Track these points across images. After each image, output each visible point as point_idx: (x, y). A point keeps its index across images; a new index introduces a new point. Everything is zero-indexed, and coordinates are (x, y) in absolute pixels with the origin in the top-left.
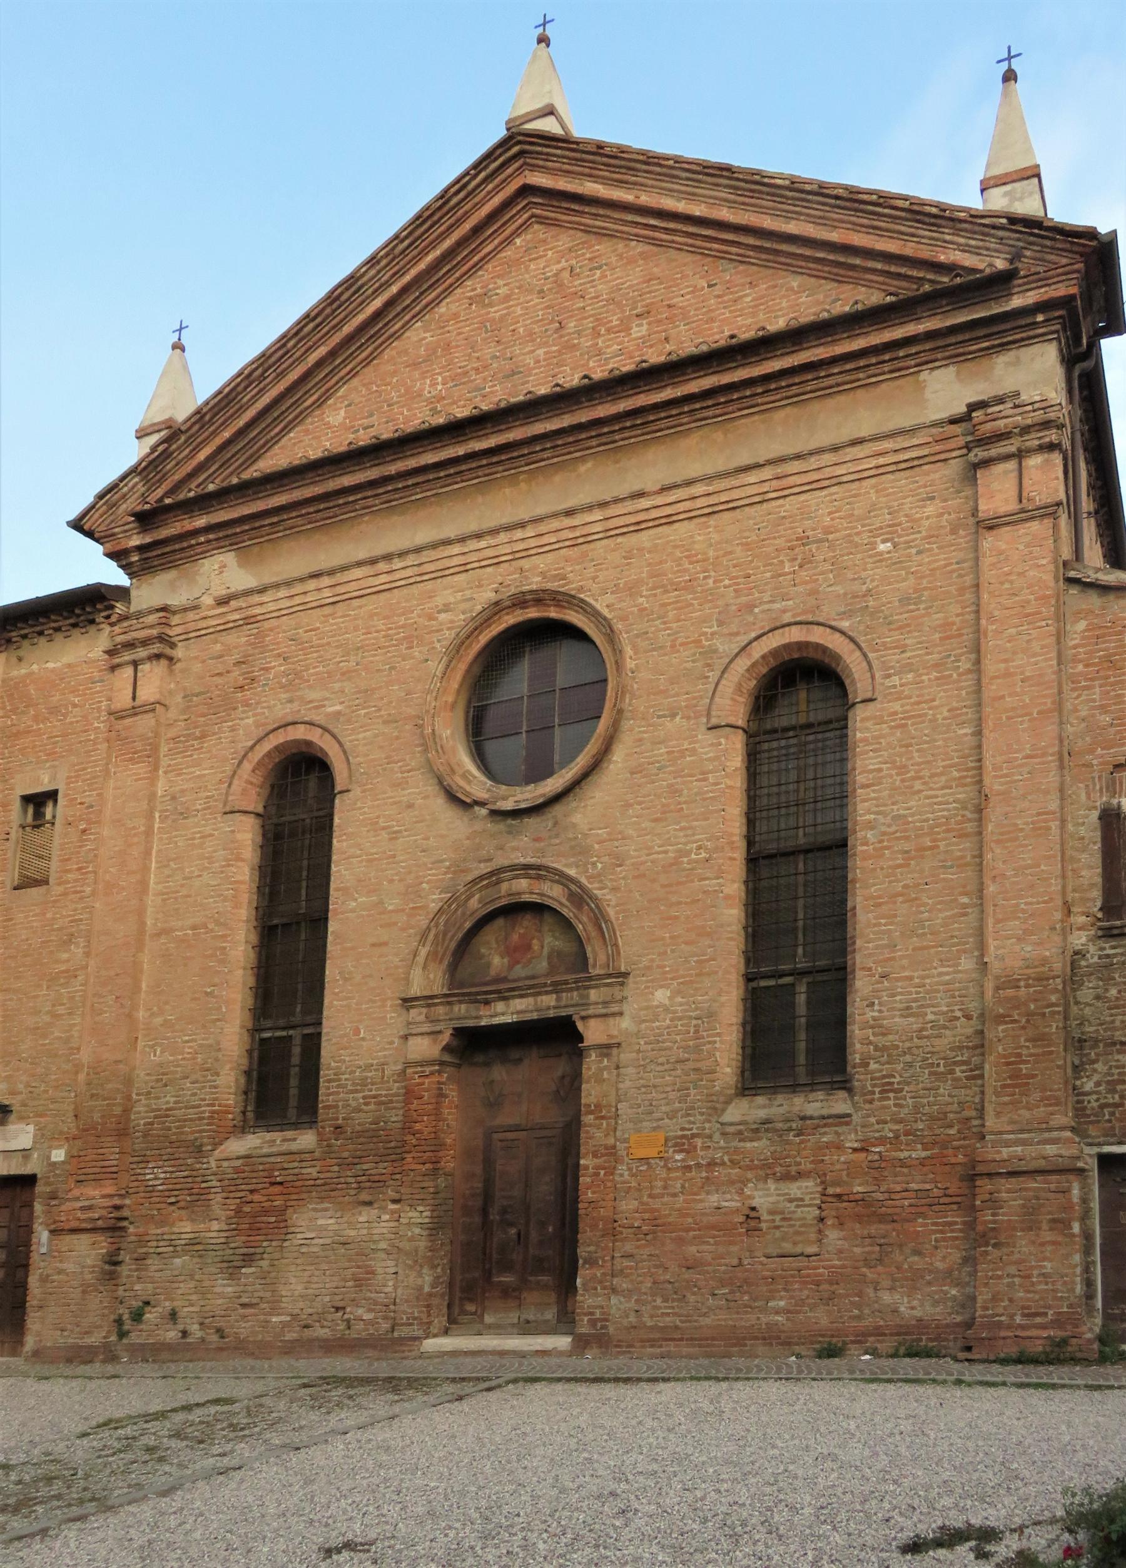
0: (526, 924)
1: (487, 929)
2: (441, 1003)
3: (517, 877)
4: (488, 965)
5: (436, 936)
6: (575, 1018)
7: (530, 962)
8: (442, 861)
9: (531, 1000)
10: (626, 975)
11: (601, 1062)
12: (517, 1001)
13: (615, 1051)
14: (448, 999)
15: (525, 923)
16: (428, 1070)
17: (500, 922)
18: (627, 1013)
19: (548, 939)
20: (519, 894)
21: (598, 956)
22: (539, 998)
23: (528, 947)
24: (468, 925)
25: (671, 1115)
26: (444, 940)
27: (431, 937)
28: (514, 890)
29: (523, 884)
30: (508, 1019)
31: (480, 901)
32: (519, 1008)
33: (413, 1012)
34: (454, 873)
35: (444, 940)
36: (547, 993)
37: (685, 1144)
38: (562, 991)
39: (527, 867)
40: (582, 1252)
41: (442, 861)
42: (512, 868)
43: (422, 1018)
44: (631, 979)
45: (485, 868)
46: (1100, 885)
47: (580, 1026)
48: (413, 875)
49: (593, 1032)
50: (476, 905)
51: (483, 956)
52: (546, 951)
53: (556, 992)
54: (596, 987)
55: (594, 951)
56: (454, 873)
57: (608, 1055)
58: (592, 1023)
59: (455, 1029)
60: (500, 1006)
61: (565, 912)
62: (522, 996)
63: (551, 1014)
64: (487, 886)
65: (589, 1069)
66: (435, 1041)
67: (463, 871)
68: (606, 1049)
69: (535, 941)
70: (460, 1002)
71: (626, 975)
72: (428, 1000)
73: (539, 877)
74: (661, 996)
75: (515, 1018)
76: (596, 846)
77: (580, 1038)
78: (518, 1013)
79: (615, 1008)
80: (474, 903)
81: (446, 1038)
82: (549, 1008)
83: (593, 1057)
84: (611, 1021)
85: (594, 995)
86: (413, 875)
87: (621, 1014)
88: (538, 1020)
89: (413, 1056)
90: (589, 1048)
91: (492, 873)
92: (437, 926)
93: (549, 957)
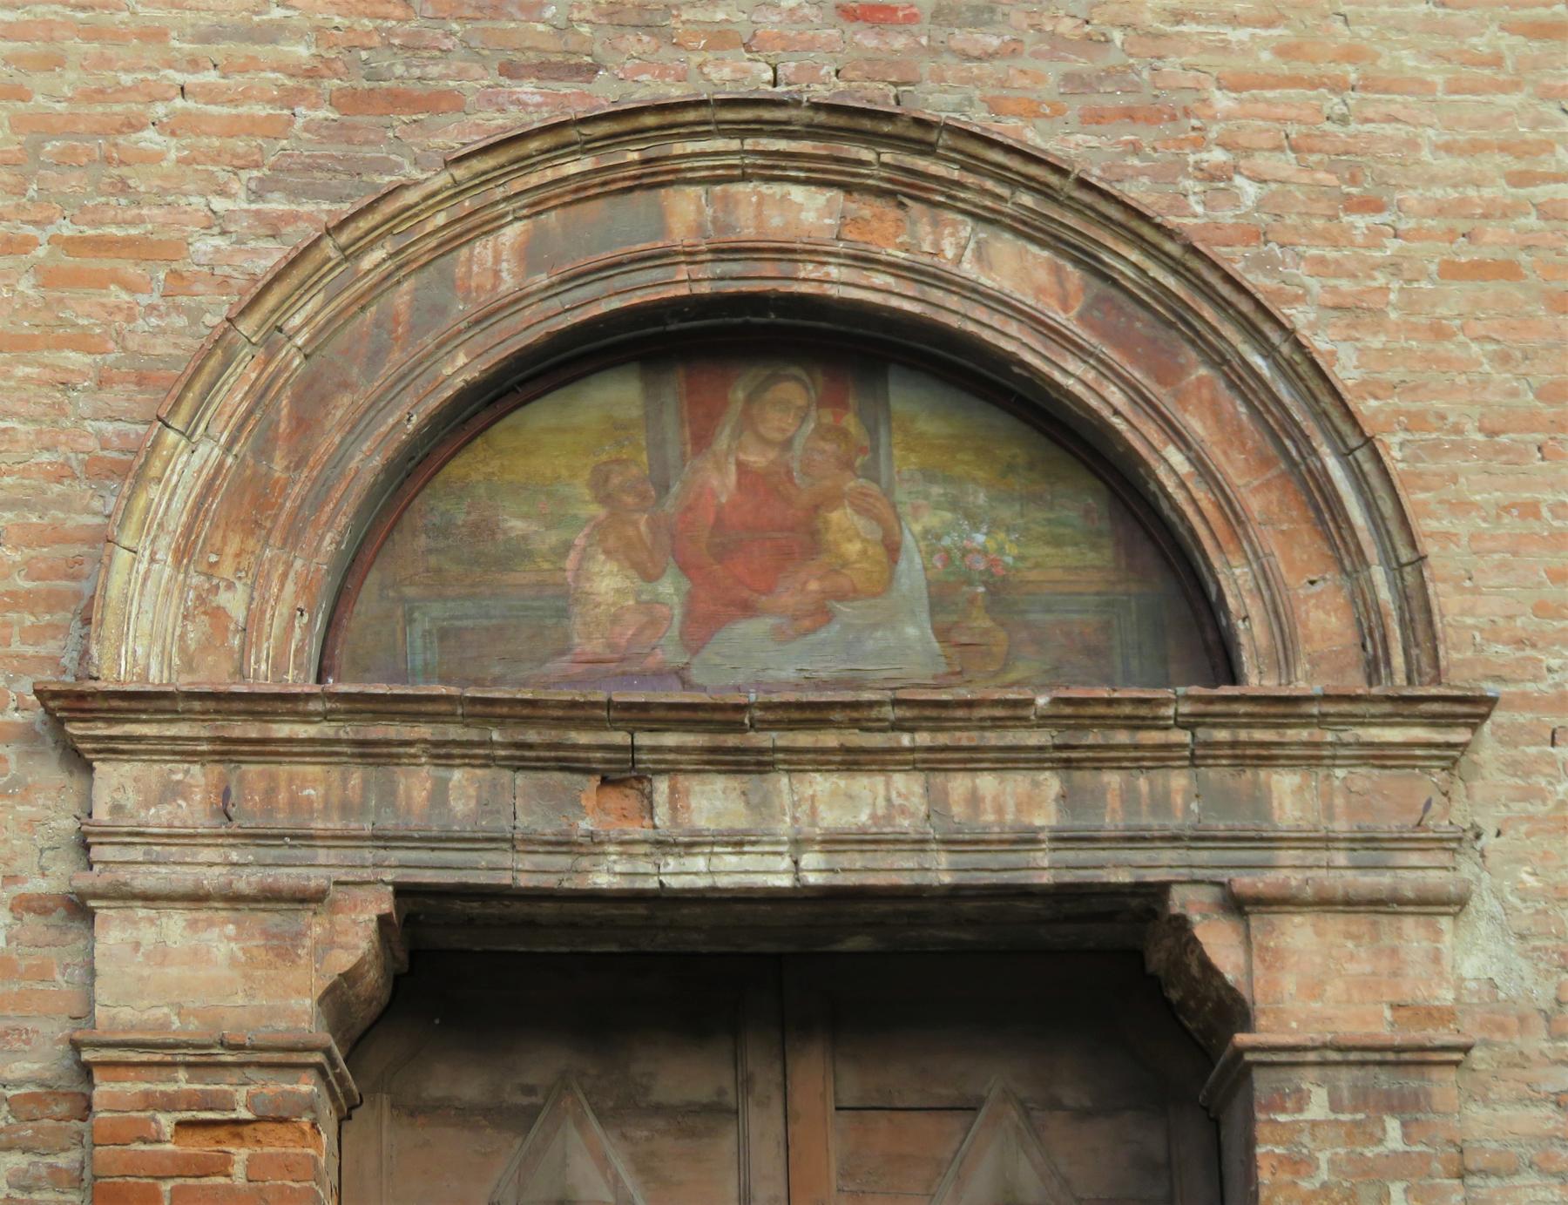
0: (779, 424)
1: (540, 416)
2: (321, 750)
3: (772, 170)
4: (563, 601)
5: (260, 396)
6: (1182, 900)
7: (822, 614)
8: (270, 34)
9: (906, 787)
10: (1473, 709)
11: (1367, 1133)
12: (821, 784)
13: (1443, 1084)
14: (374, 721)
15: (775, 422)
16: (242, 1095)
17: (616, 396)
18: (1484, 903)
19: (925, 519)
20: (784, 252)
21: (1289, 607)
22: (958, 785)
23: (803, 541)
24: (460, 368)
26: (304, 425)
27: (234, 394)
28: (746, 230)
29: (808, 210)
30: (772, 872)
31: (530, 256)
32: (831, 818)
33: (115, 782)
34: (349, 101)
35: (304, 425)
36: (1009, 760)
38: (1102, 759)
39: (847, 121)
41: (270, 34)
42: (746, 114)
43: (192, 811)
44: (1488, 746)
45: (533, 101)
46: (1256, 1109)
47: (1220, 945)
48: (70, 80)
49: (1300, 983)
50: (514, 276)
51: (519, 552)
52: (913, 570)
53: (1065, 761)
54: (1311, 759)
55: (1265, 577)
56: (349, 101)
57: (1407, 1107)
58: (1298, 935)
59: (402, 891)
60: (712, 801)
61: (1073, 376)
62: (852, 761)
63: (1043, 868)
64: (580, 192)
65: (1299, 1164)
66: (284, 949)
67: (398, 100)
68: (1400, 1065)
69: (842, 517)
70: (443, 754)
71: (1473, 709)
72: (228, 720)
73: (904, 191)
75: (815, 870)
76: (1223, 101)
77: (1233, 1010)
78: (834, 842)
79: (1418, 872)
80: (497, 258)
81: (351, 937)
82: (1027, 839)
83: (1318, 1107)
84: (1411, 933)
85: (1288, 796)
86: (70, 80)
87: (1453, 904)
88: (954, 893)
89: (124, 1008)
90: (1291, 1057)
91: (626, 122)
92: (273, 336)
93: (940, 599)
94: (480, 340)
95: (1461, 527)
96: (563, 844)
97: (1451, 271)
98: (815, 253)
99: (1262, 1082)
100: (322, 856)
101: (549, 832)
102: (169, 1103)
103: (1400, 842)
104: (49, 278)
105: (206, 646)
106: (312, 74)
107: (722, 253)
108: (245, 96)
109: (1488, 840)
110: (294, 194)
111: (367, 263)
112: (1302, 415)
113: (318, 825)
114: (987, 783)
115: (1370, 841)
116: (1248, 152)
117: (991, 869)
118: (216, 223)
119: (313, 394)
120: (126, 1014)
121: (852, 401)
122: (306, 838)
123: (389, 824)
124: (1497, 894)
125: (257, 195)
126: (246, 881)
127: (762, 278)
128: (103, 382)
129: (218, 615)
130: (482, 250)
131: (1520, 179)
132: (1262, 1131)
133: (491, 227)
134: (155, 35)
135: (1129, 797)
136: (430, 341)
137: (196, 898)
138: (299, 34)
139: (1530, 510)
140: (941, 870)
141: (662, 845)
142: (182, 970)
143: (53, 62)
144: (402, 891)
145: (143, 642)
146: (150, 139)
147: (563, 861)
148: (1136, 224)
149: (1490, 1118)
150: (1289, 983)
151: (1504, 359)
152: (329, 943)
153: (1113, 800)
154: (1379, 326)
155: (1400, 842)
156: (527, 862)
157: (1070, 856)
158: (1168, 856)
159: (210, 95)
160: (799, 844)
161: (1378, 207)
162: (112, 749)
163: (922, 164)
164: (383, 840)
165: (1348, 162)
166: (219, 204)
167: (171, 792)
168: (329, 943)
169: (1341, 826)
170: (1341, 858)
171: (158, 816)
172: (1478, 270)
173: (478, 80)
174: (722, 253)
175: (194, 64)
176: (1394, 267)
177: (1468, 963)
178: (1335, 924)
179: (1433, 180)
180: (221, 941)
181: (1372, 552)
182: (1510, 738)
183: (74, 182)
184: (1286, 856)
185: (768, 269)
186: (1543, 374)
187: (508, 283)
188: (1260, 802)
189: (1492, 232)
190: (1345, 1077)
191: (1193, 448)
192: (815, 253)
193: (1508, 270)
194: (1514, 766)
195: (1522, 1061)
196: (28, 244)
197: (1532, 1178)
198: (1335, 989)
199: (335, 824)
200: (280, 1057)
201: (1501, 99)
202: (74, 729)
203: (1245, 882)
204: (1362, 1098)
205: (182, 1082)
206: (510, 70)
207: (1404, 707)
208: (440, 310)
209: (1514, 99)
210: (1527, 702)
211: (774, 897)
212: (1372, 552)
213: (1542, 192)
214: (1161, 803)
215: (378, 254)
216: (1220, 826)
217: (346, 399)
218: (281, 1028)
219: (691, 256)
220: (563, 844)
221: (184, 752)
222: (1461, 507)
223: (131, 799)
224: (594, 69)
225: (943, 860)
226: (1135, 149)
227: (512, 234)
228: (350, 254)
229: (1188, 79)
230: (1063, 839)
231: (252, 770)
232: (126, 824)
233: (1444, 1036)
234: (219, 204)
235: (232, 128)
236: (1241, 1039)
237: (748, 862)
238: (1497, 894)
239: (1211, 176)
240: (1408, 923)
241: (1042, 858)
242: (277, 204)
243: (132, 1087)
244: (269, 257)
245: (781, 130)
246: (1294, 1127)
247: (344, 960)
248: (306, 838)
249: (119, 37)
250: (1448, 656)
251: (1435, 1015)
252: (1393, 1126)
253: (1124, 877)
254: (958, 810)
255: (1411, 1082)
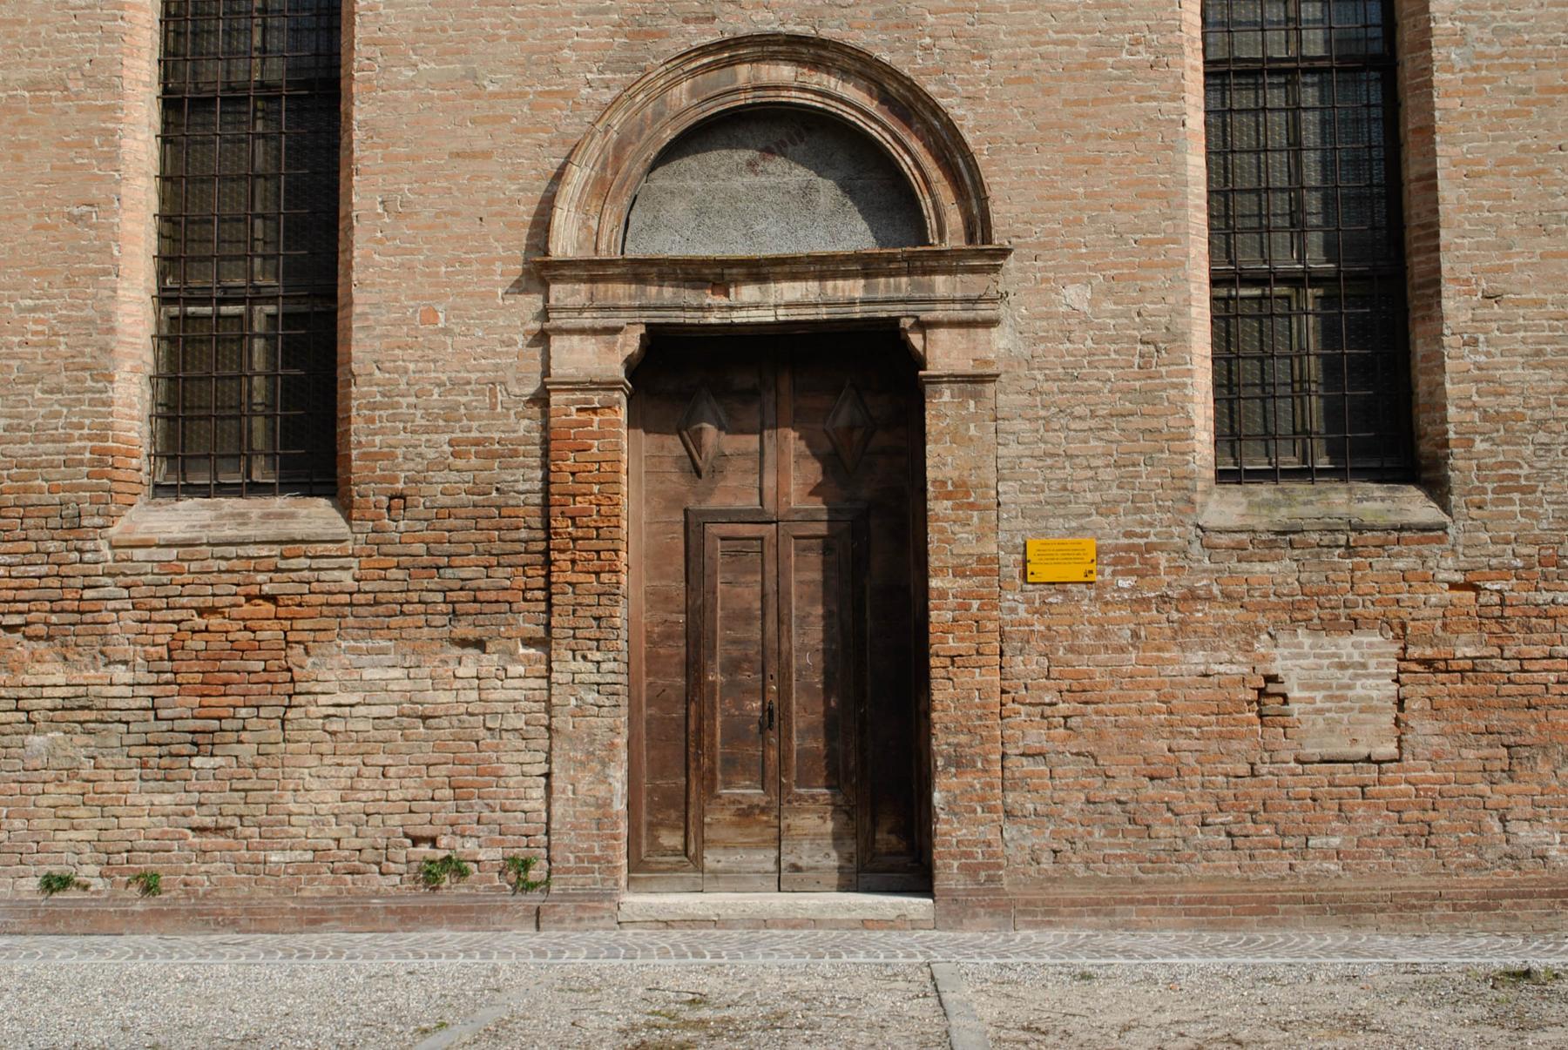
13: (989, 389)
16: (596, 399)
18: (1007, 321)
22: (830, 284)
24: (668, 135)
25: (1106, 508)
29: (784, 72)
30: (767, 316)
31: (693, 92)
33: (557, 290)
34: (635, 35)
37: (1134, 558)
40: (941, 743)
44: (1010, 263)
47: (916, 340)
49: (944, 353)
50: (685, 101)
54: (949, 271)
57: (977, 396)
58: (941, 335)
63: (858, 312)
67: (649, 34)
71: (1004, 253)
74: (1075, 295)
75: (783, 314)
76: (930, 19)
77: (919, 361)
78: (788, 305)
79: (984, 311)
81: (631, 342)
82: (852, 303)
83: (947, 397)
84: (981, 333)
85: (942, 284)
88: (828, 321)
90: (937, 380)
94: (675, 123)
95: (1006, 180)
96: (700, 308)
97: (1008, 82)
98: (788, 88)
99: (928, 388)
100: (623, 314)
101: (695, 304)
102: (575, 402)
103: (979, 300)
104: (532, 107)
105: (586, 240)
106: (620, 26)
107: (755, 89)
108: (598, 35)
109: (1011, 297)
110: (614, 72)
111: (638, 99)
112: (949, 148)
113: (622, 303)
114: (840, 283)
115: (968, 301)
116: (939, 38)
117: (840, 313)
118: (589, 83)
119: (620, 146)
120: (560, 371)
121: (785, 384)
122: (617, 308)
123: (644, 302)
124: (1013, 317)
125: (601, 72)
126: (599, 324)
127: (770, 96)
128: (551, 144)
129: (589, 228)
130: (676, 90)
131: (1035, 44)
132: (928, 406)
133: (680, 82)
134: (567, 14)
135: (887, 286)
136: (658, 126)
137: (582, 331)
138: (616, 11)
139: (1032, 172)
140: (823, 314)
141: (731, 308)
142: (580, 357)
143: (534, 26)
144: (647, 325)
145: (565, 242)
146: (566, 53)
147: (700, 314)
148: (895, 74)
149: (1006, 398)
150: (938, 352)
151: (1025, 114)
152: (624, 345)
153: (882, 287)
154: (982, 104)
155: (979, 300)
156: (688, 314)
157: (866, 308)
158: (900, 307)
159: (586, 35)
160: (776, 306)
161: (983, 58)
162: (556, 279)
163: (823, 53)
164: (641, 308)
165: (973, 40)
166: (589, 76)
167: (573, 293)
168: (624, 345)
169: (958, 295)
170: (958, 306)
171: (570, 302)
172: (1018, 81)
173: (676, 24)
174: (755, 89)
175: (581, 24)
176: (988, 81)
177: (999, 342)
178: (955, 331)
179: (1004, 46)
180: (591, 344)
181: (972, 194)
182: (1020, 259)
183: (542, 70)
184: (939, 306)
185: (772, 93)
186: (1039, 119)
187: (685, 103)
188: (931, 288)
189: (1024, 65)
190: (955, 386)
191: (913, 155)
192: (788, 88)
193: (1028, 80)
194: (1020, 270)
195: (1018, 378)
196: (527, 94)
197: (1020, 420)
198: (954, 354)
199: (627, 303)
200: (610, 386)
201: (1030, 12)
202: (544, 273)
203: (924, 316)
204: (962, 393)
205: (579, 395)
206: (686, 21)
207: (980, 254)
208: (662, 114)
209: (1034, 13)
210: (1027, 245)
211: (768, 324)
212: (972, 194)
213: (1042, 49)
214: (898, 288)
215: (641, 96)
216: (917, 295)
217: (630, 149)
218: (607, 376)
219: (745, 90)
220: (700, 308)
221: (580, 280)
222: (1006, 172)
223: (561, 296)
224: (714, 18)
225: (824, 310)
226: (899, 40)
227: (685, 85)
228: (631, 98)
229: (919, 11)
230: (863, 302)
231: (601, 286)
232: (561, 304)
233: (989, 371)
234: (589, 76)
235: (594, 48)
236: (921, 373)
237: (760, 313)
238: (1013, 317)
239: (925, 48)
240: (980, 331)
241: (857, 309)
242: (609, 76)
243: (563, 397)
244: (607, 97)
245: (776, 43)
246: (939, 404)
247: (629, 351)
248: (617, 308)
249: (556, 16)
250: (995, 235)
251: (987, 363)
252: (972, 403)
253: (884, 315)
254: (830, 292)
255: (979, 387)
